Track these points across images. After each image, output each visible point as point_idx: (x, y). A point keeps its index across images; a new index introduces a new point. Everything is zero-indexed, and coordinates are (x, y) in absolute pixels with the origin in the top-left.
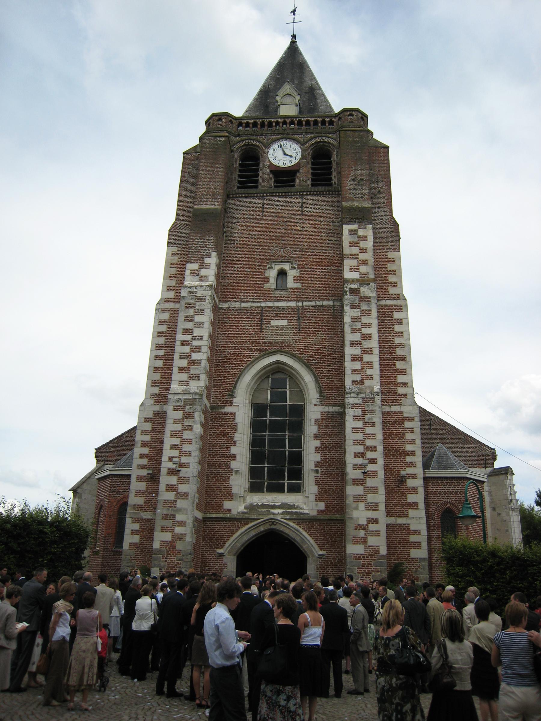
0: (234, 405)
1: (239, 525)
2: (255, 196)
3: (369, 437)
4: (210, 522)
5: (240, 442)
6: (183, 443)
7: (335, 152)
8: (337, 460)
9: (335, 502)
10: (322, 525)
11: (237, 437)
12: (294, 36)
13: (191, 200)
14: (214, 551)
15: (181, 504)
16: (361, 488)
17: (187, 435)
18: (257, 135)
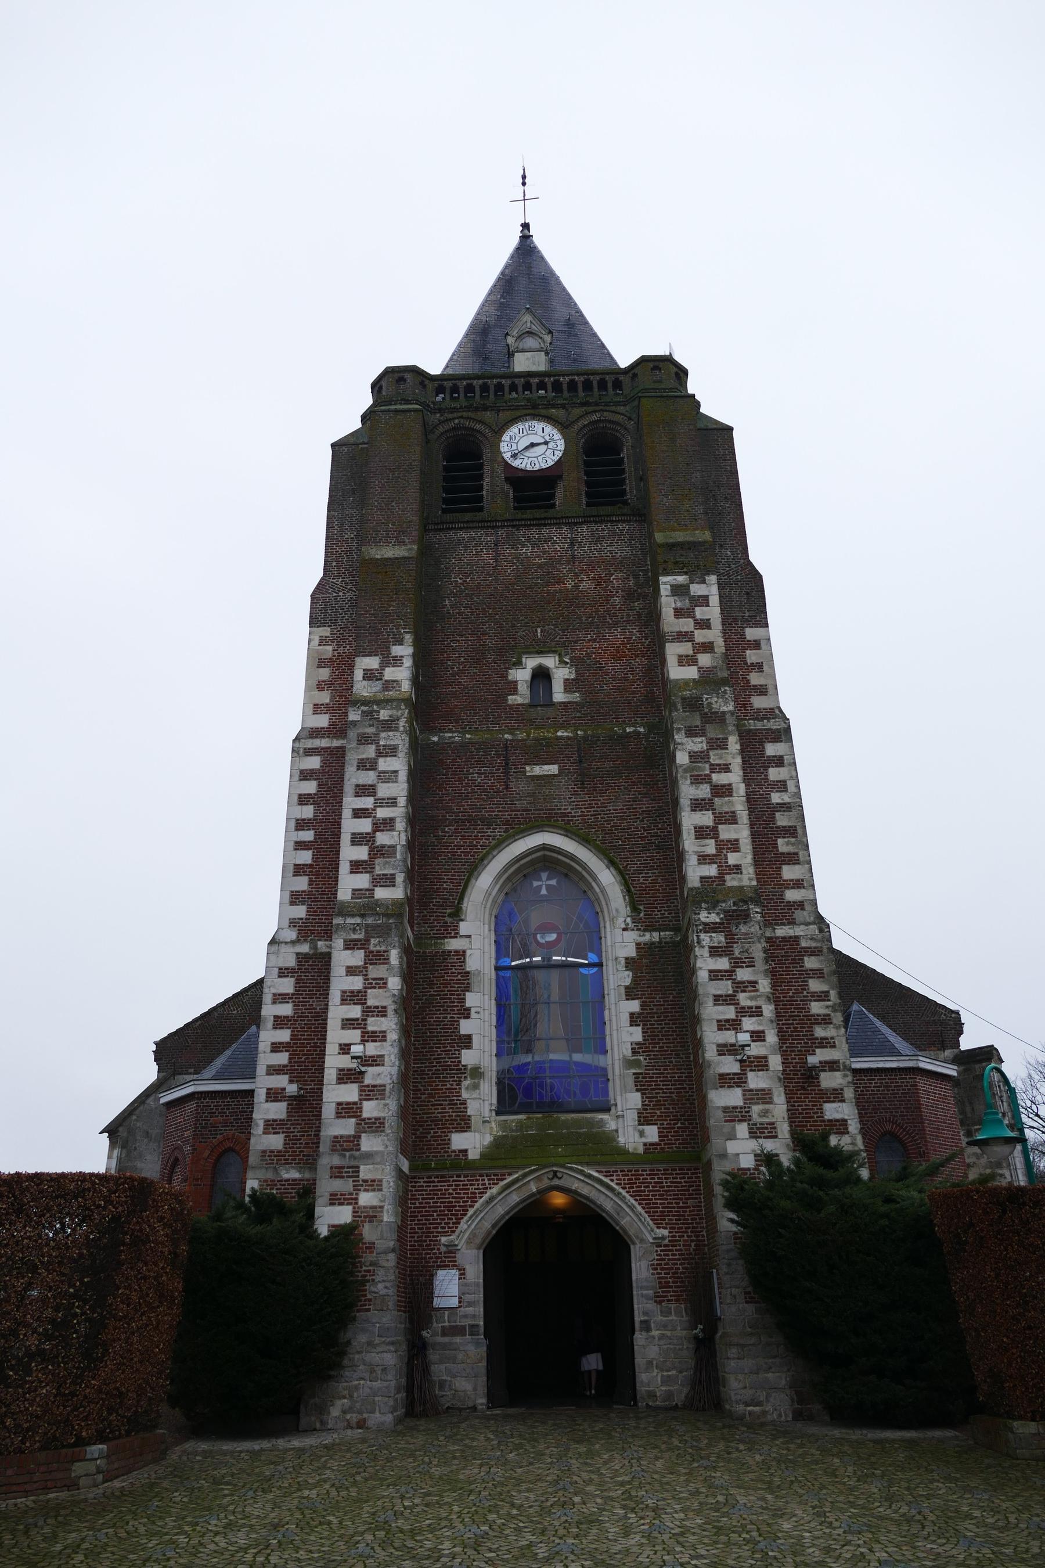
0: (461, 936)
1: (487, 1182)
2: (479, 527)
3: (744, 987)
4: (425, 1180)
5: (478, 1009)
6: (368, 1016)
7: (628, 441)
8: (676, 1039)
9: (679, 1125)
10: (656, 1175)
11: (472, 1000)
12: (526, 226)
13: (352, 536)
14: (437, 1241)
15: (368, 1143)
16: (738, 1092)
17: (375, 998)
18: (476, 409)
